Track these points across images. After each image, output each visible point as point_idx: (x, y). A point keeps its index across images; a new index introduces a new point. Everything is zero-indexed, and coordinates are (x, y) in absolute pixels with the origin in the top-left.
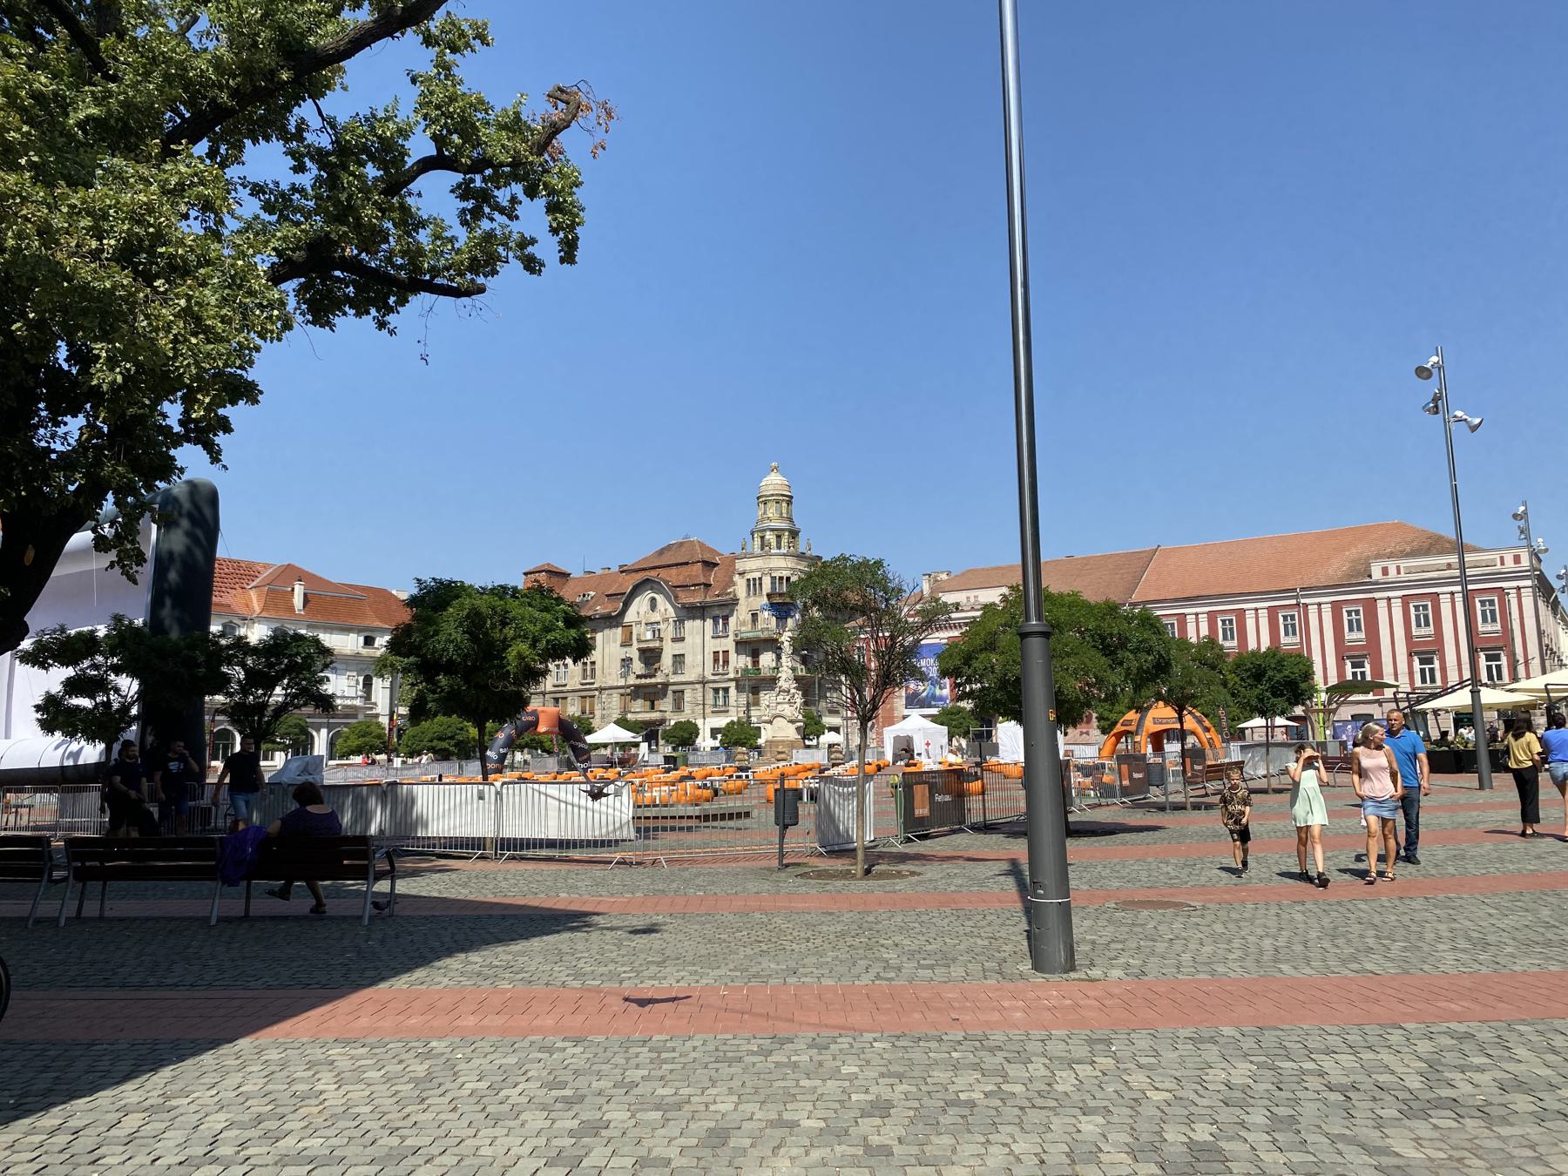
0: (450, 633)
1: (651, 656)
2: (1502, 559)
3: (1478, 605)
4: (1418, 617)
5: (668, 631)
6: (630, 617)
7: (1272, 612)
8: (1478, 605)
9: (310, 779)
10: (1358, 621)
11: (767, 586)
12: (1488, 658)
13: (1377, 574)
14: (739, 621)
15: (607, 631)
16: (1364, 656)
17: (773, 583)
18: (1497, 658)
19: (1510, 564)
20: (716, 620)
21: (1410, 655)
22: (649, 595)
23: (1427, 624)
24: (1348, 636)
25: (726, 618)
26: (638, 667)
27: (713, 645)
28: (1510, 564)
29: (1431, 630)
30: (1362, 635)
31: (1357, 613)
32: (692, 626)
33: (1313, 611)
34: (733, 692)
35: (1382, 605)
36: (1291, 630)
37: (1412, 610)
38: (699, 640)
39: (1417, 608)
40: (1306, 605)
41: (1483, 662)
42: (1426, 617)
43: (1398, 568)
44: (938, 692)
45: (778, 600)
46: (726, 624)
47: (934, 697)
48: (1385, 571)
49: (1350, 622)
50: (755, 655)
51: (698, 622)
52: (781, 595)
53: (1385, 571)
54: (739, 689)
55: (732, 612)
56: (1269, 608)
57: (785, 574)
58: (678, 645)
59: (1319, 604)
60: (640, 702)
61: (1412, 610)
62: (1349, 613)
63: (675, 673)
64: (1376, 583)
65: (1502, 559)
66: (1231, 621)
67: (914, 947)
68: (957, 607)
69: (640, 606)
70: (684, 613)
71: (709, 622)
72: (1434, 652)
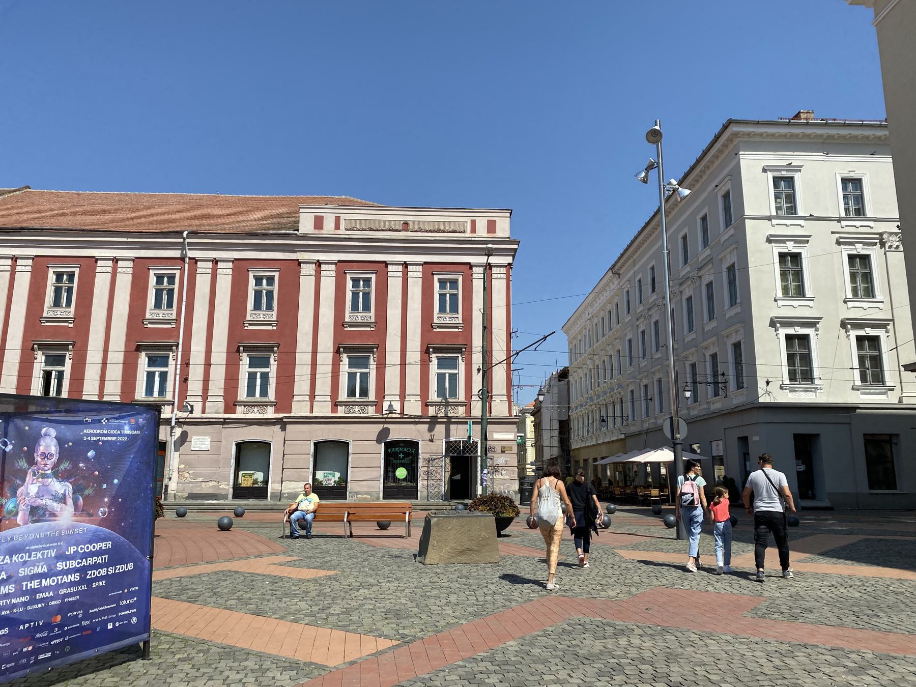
0: (652, 138)
2: (473, 223)
3: (252, 282)
4: (355, 295)
7: (141, 267)
8: (252, 282)
9: (11, 543)
10: (270, 294)
12: (152, 361)
13: (306, 226)
16: (270, 349)
18: (60, 361)
19: (482, 232)
21: (337, 352)
23: (367, 308)
24: (250, 313)
28: (482, 232)
29: (459, 318)
30: (273, 316)
31: (270, 280)
33: (204, 269)
35: (307, 271)
36: (164, 298)
37: (349, 284)
39: (355, 281)
40: (195, 261)
41: (40, 360)
42: (367, 295)
43: (338, 220)
48: (319, 222)
49: (258, 294)
53: (319, 222)
56: (135, 260)
59: (215, 262)
61: (349, 284)
62: (258, 280)
64: (305, 237)
65: (337, 227)
66: (71, 276)
72: (369, 350)
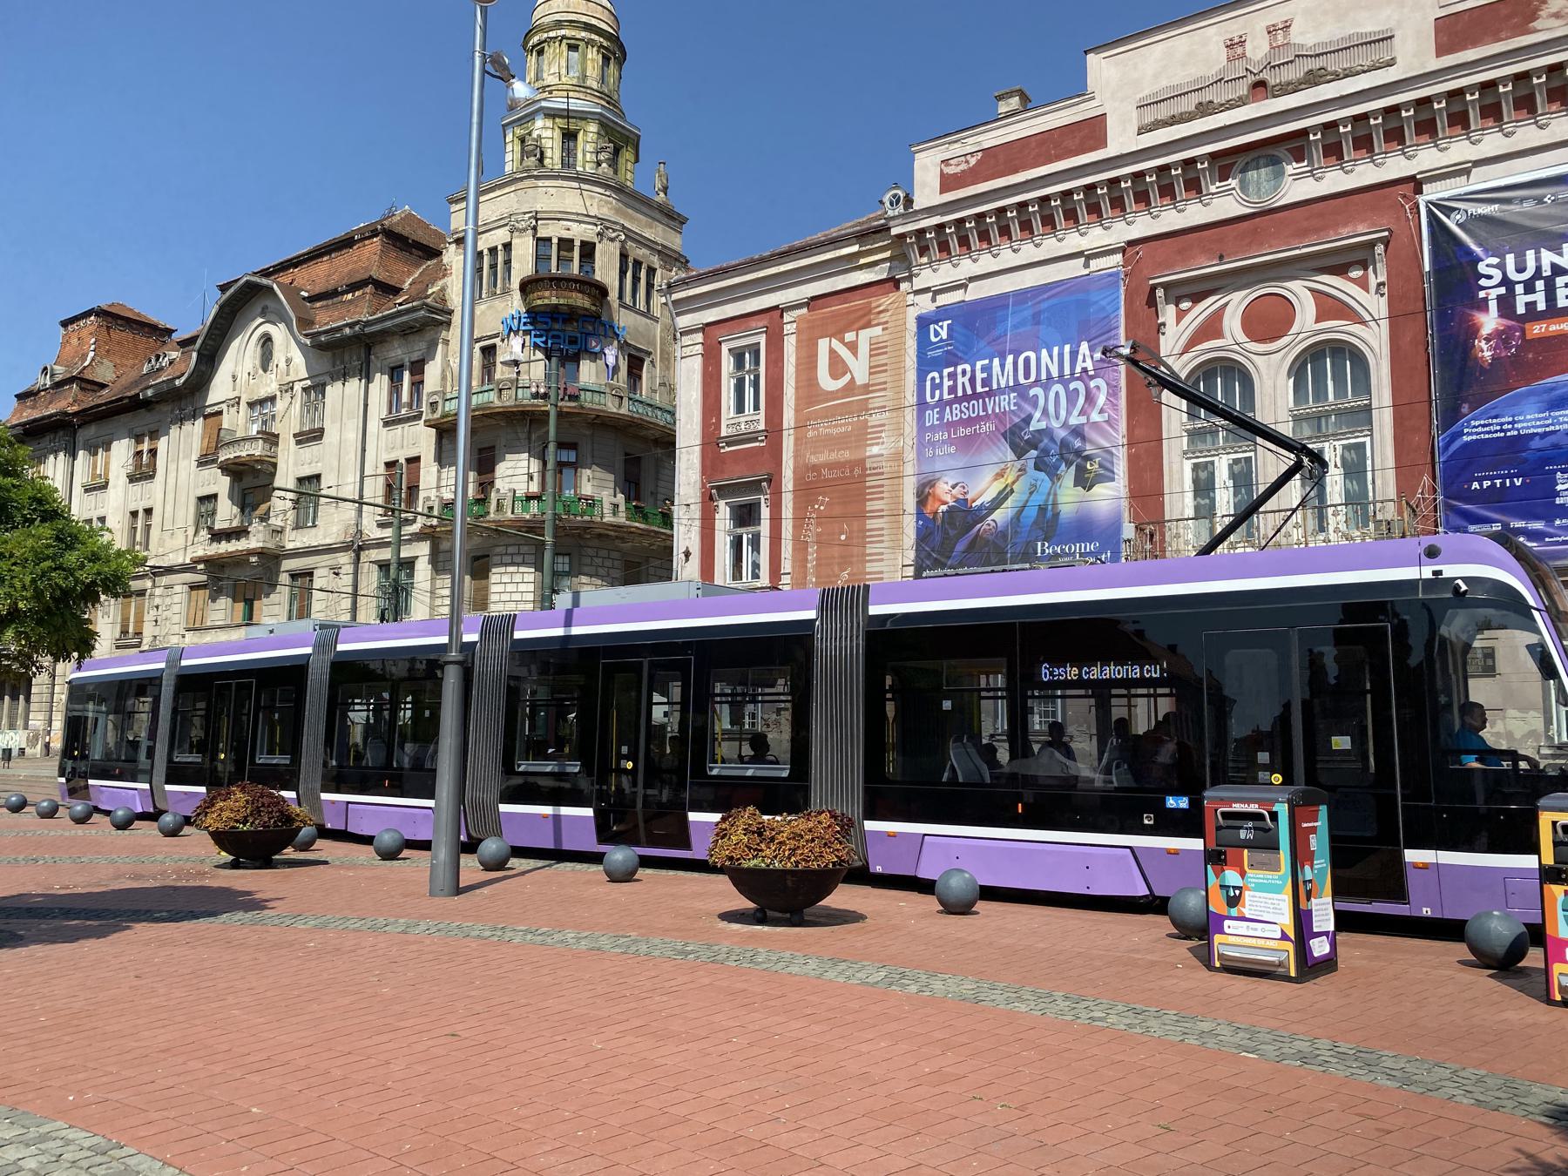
1: (251, 482)
5: (289, 417)
6: (219, 390)
11: (523, 264)
14: (447, 370)
15: (174, 431)
17: (541, 258)
20: (395, 373)
22: (258, 327)
25: (418, 368)
26: (227, 515)
27: (390, 444)
32: (343, 395)
34: (423, 569)
38: (353, 436)
44: (1068, 497)
45: (549, 298)
46: (417, 385)
47: (1048, 523)
50: (484, 463)
51: (354, 385)
52: (558, 282)
54: (439, 562)
55: (432, 346)
57: (580, 232)
58: (311, 451)
60: (224, 602)
63: (297, 527)
67: (518, 148)
68: (1002, 366)
69: (239, 357)
70: (324, 364)
71: (381, 383)
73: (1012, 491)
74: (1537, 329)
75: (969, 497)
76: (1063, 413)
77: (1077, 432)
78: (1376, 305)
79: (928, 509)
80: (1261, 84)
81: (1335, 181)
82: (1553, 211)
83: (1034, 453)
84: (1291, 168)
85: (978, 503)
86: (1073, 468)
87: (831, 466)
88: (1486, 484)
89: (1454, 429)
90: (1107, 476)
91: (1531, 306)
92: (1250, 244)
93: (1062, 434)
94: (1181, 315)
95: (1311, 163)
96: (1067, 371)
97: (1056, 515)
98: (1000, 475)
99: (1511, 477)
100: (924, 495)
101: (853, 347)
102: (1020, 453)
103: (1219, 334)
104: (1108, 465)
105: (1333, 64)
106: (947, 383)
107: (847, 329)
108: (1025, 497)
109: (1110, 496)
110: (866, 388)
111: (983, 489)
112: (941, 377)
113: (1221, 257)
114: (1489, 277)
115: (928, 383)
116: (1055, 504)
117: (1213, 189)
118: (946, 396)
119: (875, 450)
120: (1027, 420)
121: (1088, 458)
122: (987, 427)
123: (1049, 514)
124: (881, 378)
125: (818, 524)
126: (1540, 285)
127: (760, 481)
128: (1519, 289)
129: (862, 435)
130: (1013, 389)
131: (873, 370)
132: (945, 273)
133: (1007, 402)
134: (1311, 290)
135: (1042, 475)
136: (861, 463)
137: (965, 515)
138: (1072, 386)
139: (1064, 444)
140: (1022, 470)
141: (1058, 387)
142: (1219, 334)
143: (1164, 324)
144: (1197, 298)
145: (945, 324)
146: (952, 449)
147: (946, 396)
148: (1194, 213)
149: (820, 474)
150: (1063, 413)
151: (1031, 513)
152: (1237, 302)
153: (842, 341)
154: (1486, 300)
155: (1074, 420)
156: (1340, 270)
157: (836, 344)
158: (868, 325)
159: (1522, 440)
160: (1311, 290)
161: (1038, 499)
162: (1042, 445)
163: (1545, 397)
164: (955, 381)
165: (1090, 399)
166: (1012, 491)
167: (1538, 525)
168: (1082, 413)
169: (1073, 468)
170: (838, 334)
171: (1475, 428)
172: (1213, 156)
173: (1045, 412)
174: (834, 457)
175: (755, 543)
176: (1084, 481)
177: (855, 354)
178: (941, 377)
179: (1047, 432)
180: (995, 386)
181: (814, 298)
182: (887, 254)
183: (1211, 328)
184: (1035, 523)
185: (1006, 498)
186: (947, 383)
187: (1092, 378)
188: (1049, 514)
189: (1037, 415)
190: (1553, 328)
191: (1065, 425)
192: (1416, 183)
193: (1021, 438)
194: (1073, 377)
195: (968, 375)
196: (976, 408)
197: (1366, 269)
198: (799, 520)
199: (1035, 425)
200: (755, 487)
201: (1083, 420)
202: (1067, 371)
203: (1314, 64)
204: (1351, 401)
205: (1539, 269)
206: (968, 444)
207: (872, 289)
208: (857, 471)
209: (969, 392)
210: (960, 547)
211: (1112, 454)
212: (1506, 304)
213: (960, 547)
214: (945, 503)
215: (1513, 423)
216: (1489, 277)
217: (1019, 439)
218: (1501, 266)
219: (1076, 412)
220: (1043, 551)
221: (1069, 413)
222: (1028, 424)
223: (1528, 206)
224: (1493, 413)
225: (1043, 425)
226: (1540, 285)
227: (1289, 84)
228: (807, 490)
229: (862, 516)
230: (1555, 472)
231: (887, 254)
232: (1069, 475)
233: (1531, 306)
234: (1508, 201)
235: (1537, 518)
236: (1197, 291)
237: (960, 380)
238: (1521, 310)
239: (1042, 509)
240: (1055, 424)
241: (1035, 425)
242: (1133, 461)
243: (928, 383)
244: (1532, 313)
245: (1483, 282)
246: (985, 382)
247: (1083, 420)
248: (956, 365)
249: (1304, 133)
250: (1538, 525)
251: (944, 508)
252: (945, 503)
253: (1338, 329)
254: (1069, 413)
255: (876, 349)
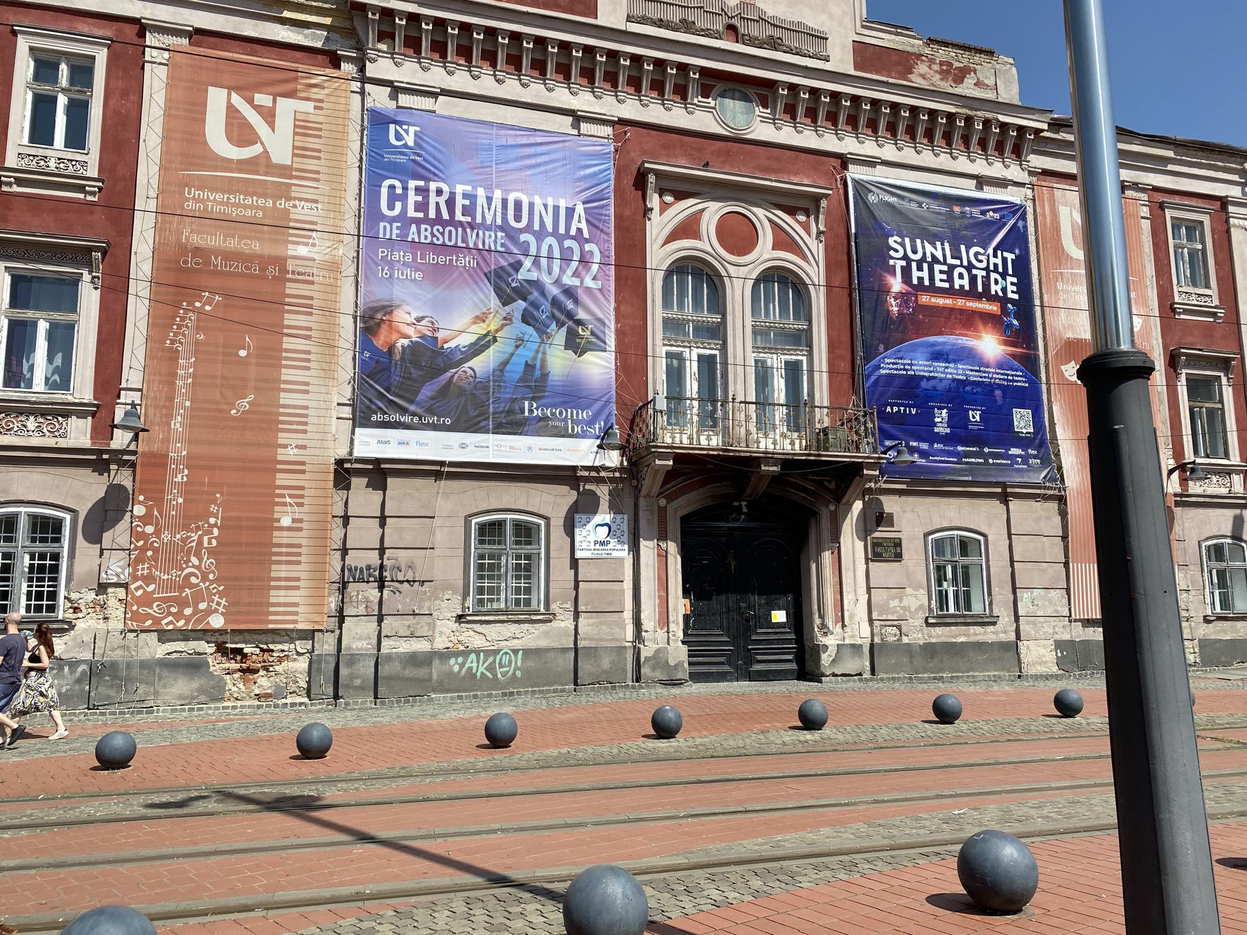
44: (558, 360)
47: (535, 381)
73: (495, 340)
74: (925, 299)
75: (441, 335)
76: (556, 269)
77: (569, 292)
78: (817, 248)
79: (380, 341)
80: (732, 28)
81: (786, 135)
82: (926, 214)
83: (521, 304)
84: (759, 110)
85: (452, 344)
86: (564, 329)
87: (229, 256)
88: (895, 409)
89: (873, 363)
90: (597, 344)
91: (920, 279)
92: (724, 162)
93: (554, 291)
94: (664, 207)
95: (774, 112)
96: (562, 230)
97: (545, 376)
98: (481, 319)
99: (910, 406)
100: (372, 321)
101: (269, 115)
102: (506, 301)
103: (696, 235)
104: (601, 335)
105: (788, 40)
106: (413, 198)
107: (260, 87)
108: (511, 349)
109: (599, 367)
110: (284, 171)
111: (459, 330)
112: (405, 189)
113: (707, 164)
114: (897, 251)
115: (384, 191)
116: (543, 361)
117: (696, 101)
118: (411, 213)
119: (302, 251)
120: (517, 266)
121: (579, 323)
122: (466, 261)
123: (537, 373)
124: (312, 165)
125: (198, 329)
126: (925, 266)
127: (90, 250)
128: (914, 265)
129: (281, 226)
130: (501, 228)
131: (299, 152)
132: (408, 72)
133: (494, 240)
134: (770, 221)
135: (530, 330)
136: (281, 262)
137: (430, 358)
138: (568, 243)
139: (555, 302)
140: (508, 319)
141: (550, 240)
142: (696, 235)
143: (651, 210)
144: (680, 196)
145: (412, 129)
146: (418, 276)
147: (411, 213)
148: (676, 116)
149: (208, 263)
150: (556, 269)
151: (516, 370)
152: (713, 212)
153: (250, 101)
154: (894, 267)
155: (568, 280)
156: (791, 211)
157: (236, 99)
158: (291, 94)
159: (914, 380)
160: (770, 221)
161: (526, 353)
162: (531, 298)
163: (930, 349)
164: (426, 197)
165: (585, 261)
166: (495, 340)
167: (924, 446)
168: (576, 274)
169: (564, 329)
170: (246, 90)
171: (888, 365)
172: (704, 71)
173: (536, 263)
174: (232, 244)
175: (62, 339)
176: (575, 344)
177: (272, 125)
178: (405, 189)
179: (537, 285)
180: (479, 220)
181: (199, 31)
182: (327, 21)
183: (688, 229)
184: (520, 380)
185: (486, 346)
186: (413, 198)
187: (587, 241)
188: (537, 373)
189: (527, 263)
190: (933, 300)
191: (557, 282)
192: (844, 161)
193: (509, 285)
194: (567, 235)
195: (445, 196)
196: (454, 237)
197: (808, 217)
198: (160, 324)
199: (522, 275)
200: (81, 256)
201: (576, 282)
202: (562, 230)
203: (777, 33)
204: (793, 324)
205: (924, 254)
206: (437, 274)
207: (298, 54)
208: (272, 271)
209: (446, 216)
210: (426, 392)
211: (604, 324)
212: (906, 272)
213: (426, 392)
214: (406, 337)
215: (911, 365)
216: (897, 251)
217: (507, 287)
218: (903, 245)
219: (569, 272)
220: (531, 411)
221: (562, 271)
222: (517, 271)
223: (914, 206)
224: (900, 355)
225: (534, 276)
226: (925, 266)
227: (756, 38)
228: (181, 277)
229: (278, 331)
230: (933, 408)
231: (327, 21)
232: (560, 336)
233: (920, 279)
234: (902, 198)
235: (924, 441)
236: (680, 189)
237: (433, 199)
238: (915, 281)
239: (529, 367)
240: (547, 280)
241: (522, 275)
242: (620, 334)
243: (384, 191)
244: (920, 287)
245: (892, 253)
246: (466, 211)
247: (576, 282)
248: (427, 180)
249: (772, 84)
250: (924, 446)
251: (406, 342)
252: (406, 337)
253: (787, 259)
254: (562, 271)
255: (302, 128)
